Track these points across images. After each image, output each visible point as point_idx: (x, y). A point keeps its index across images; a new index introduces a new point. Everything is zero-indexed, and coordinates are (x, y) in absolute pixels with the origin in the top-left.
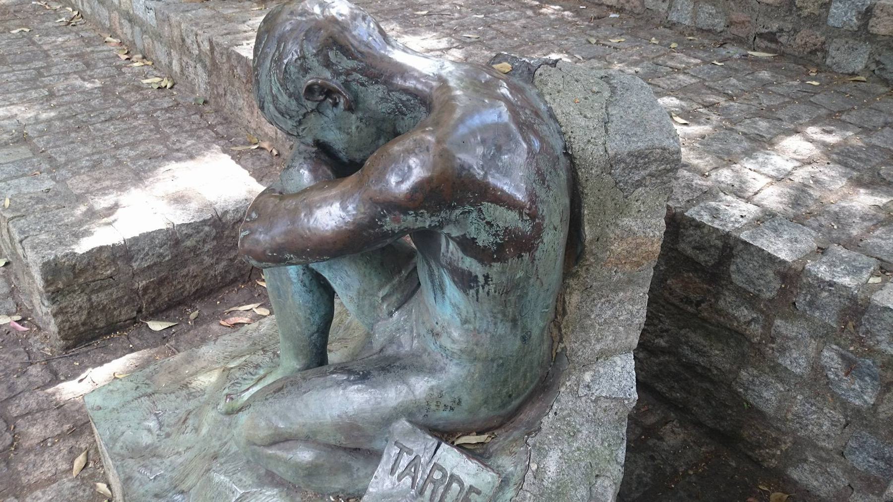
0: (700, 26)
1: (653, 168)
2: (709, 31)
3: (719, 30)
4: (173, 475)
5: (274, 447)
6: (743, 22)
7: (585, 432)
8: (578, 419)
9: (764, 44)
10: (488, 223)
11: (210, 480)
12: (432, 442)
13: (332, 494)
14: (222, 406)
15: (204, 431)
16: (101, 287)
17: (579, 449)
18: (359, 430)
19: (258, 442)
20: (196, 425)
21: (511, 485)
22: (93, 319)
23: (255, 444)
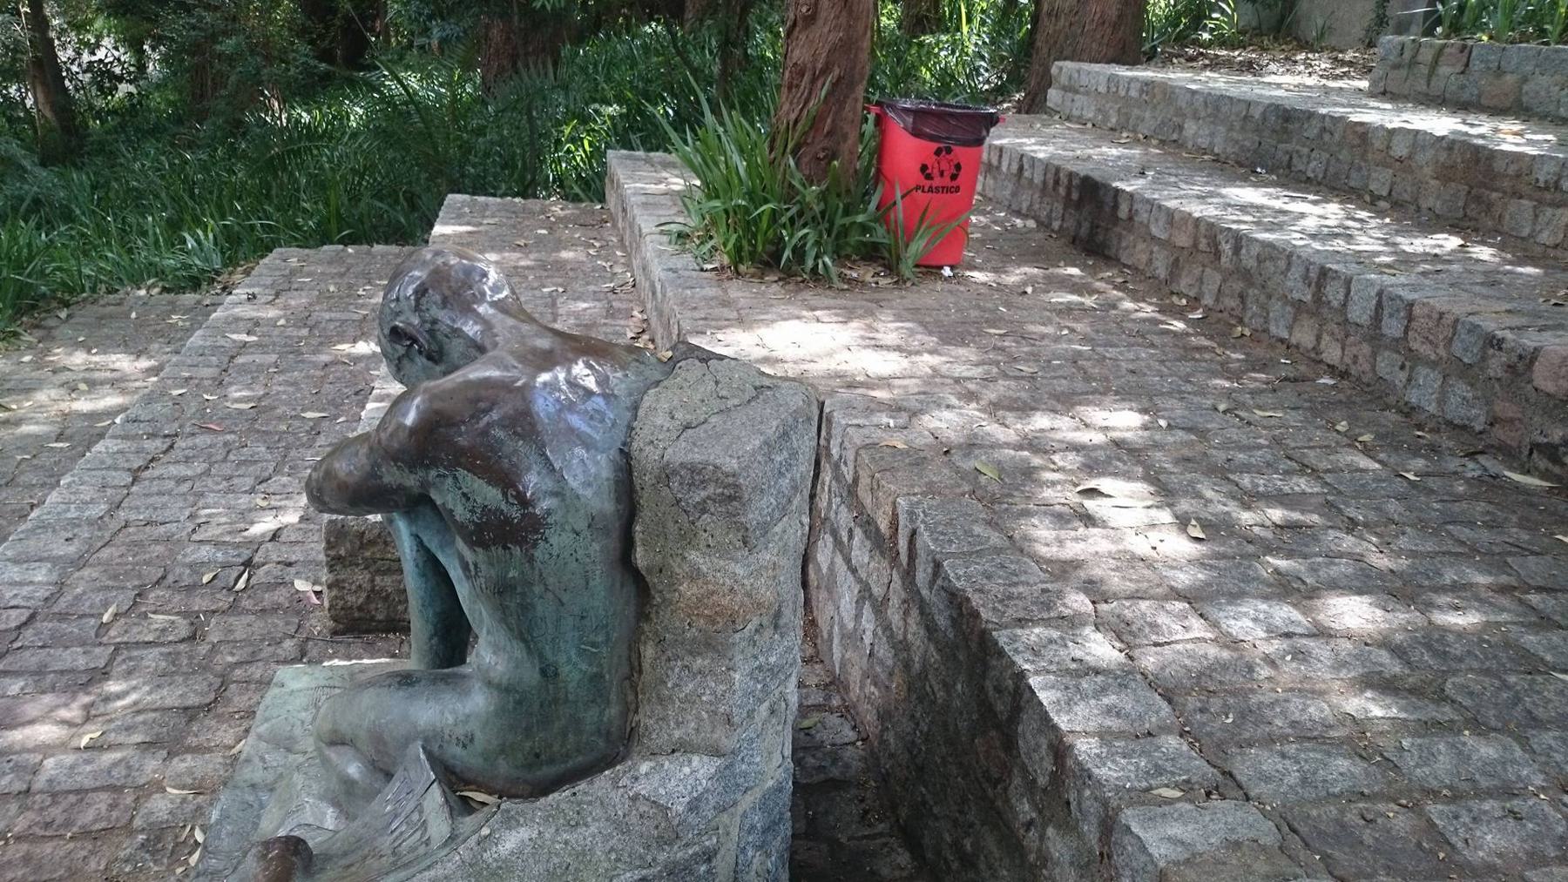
0: (1448, 417)
1: (711, 490)
2: (1464, 427)
3: (1478, 428)
6: (1512, 421)
7: (593, 829)
8: (598, 812)
9: (1543, 464)
10: (464, 494)
16: (389, 569)
17: (566, 843)
22: (372, 606)
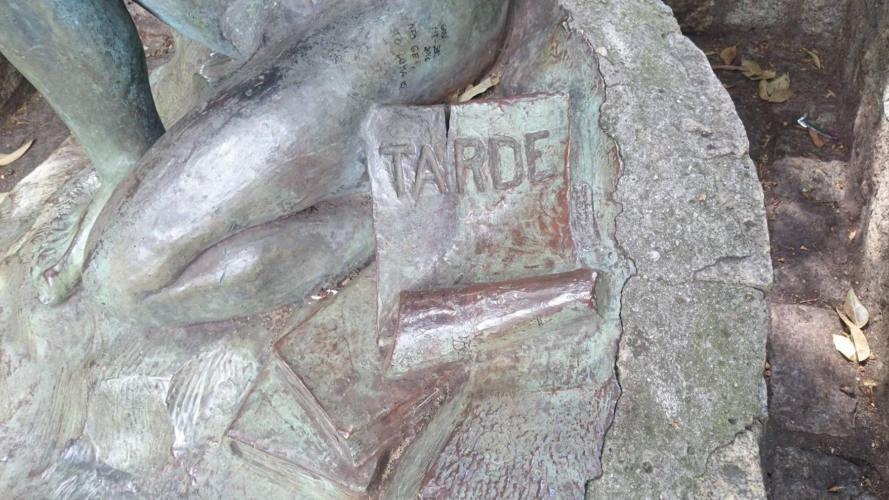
4: (37, 433)
5: (183, 278)
11: (106, 396)
12: (433, 113)
13: (313, 292)
14: (48, 292)
15: (41, 349)
18: (313, 166)
19: (153, 286)
20: (22, 350)
21: (588, 92)
23: (149, 293)
